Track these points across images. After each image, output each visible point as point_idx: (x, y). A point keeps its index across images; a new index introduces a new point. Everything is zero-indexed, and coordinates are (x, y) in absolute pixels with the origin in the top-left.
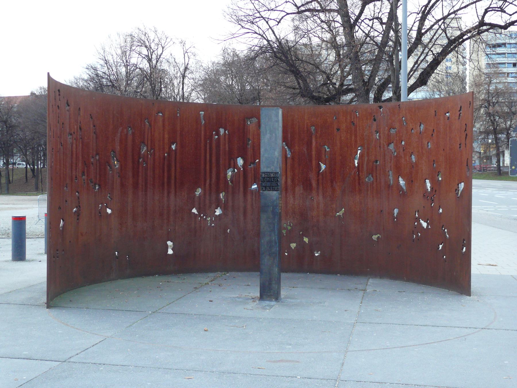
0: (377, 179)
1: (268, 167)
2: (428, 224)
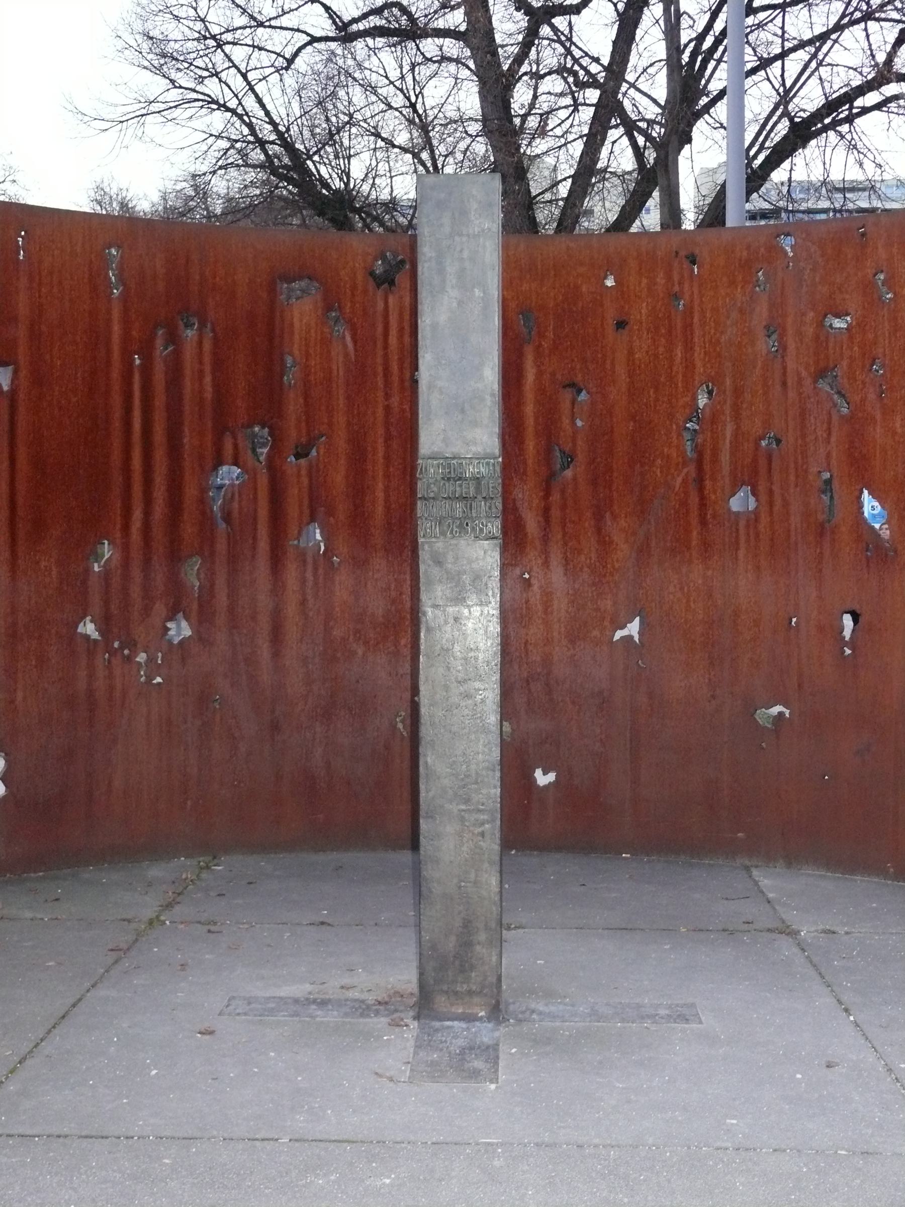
0: (771, 504)
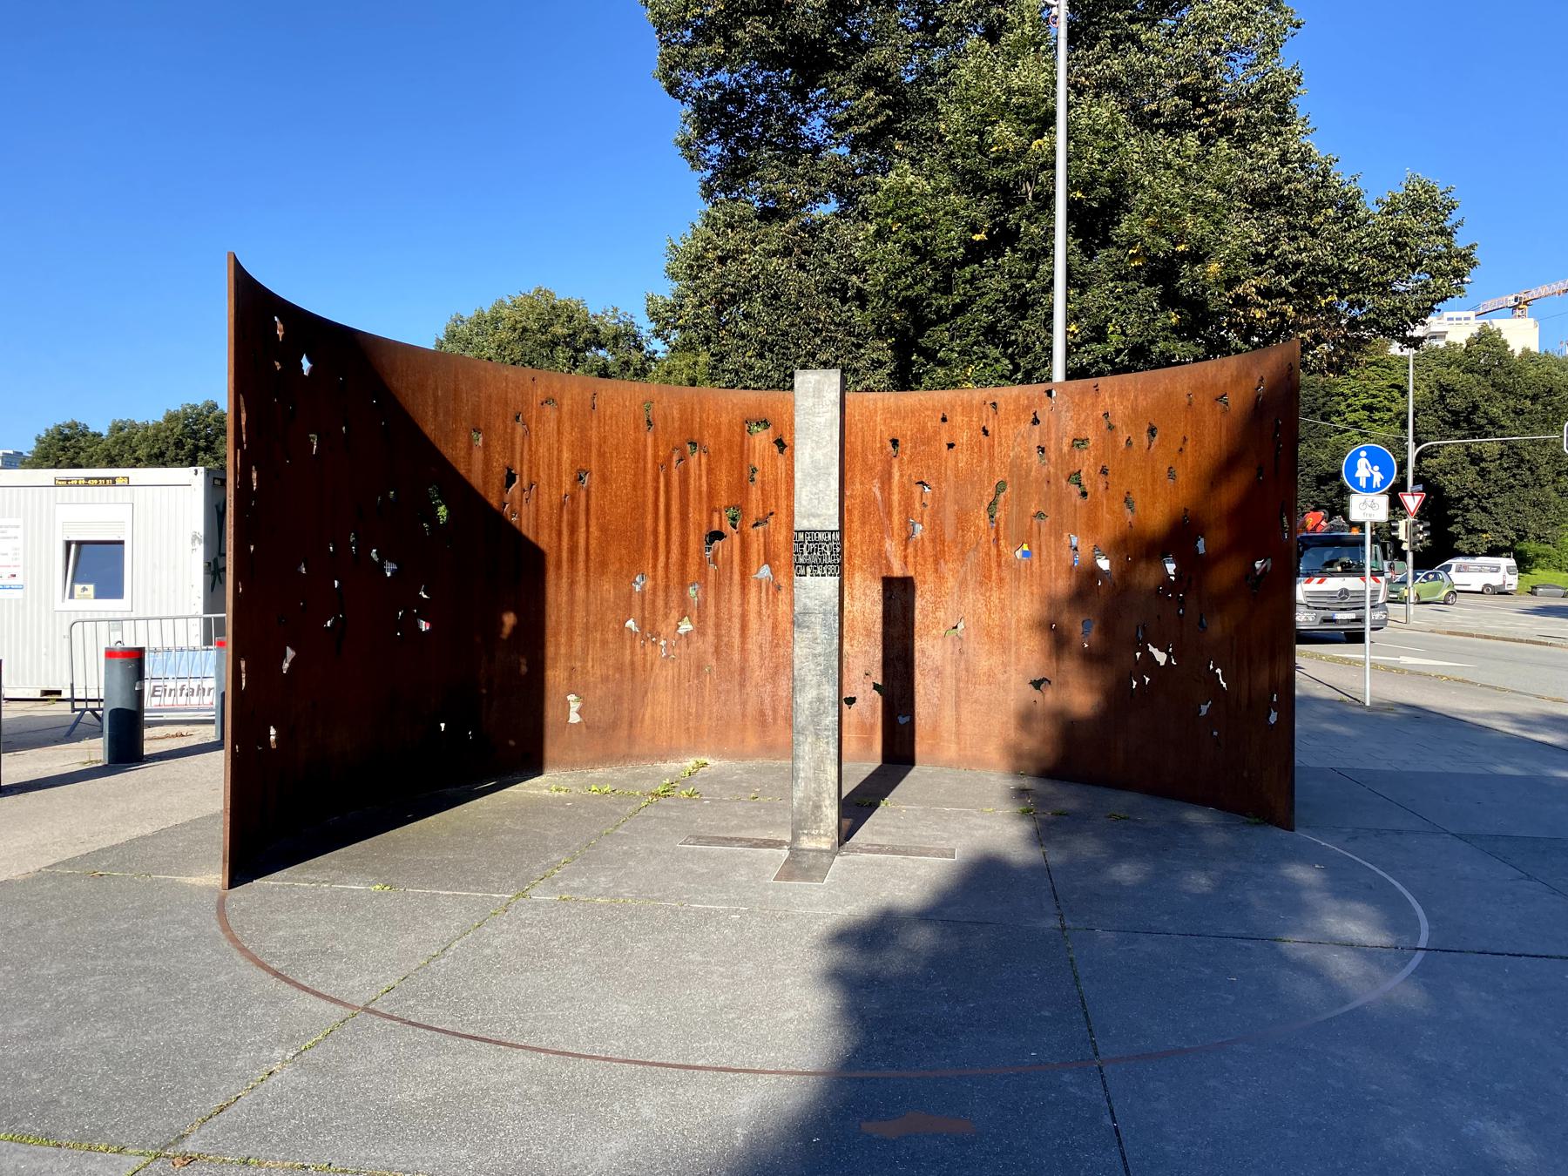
2: (1169, 655)
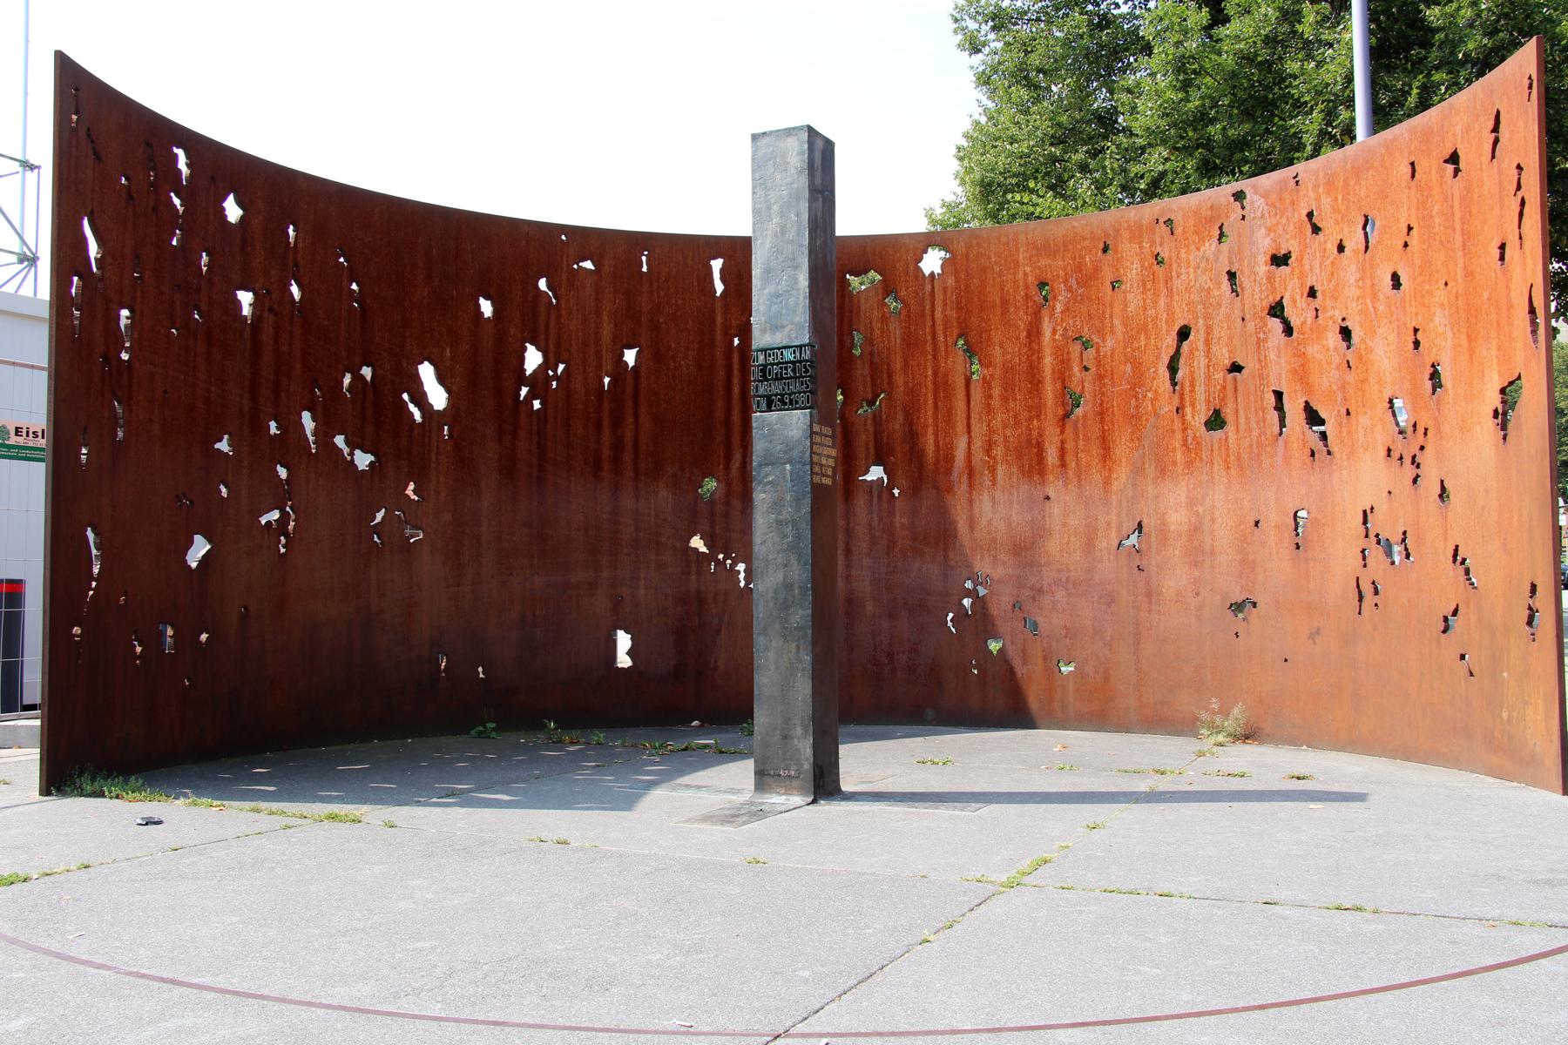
1: (775, 328)
